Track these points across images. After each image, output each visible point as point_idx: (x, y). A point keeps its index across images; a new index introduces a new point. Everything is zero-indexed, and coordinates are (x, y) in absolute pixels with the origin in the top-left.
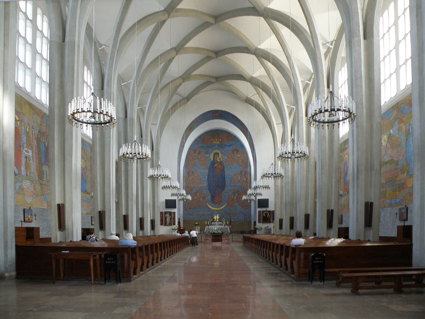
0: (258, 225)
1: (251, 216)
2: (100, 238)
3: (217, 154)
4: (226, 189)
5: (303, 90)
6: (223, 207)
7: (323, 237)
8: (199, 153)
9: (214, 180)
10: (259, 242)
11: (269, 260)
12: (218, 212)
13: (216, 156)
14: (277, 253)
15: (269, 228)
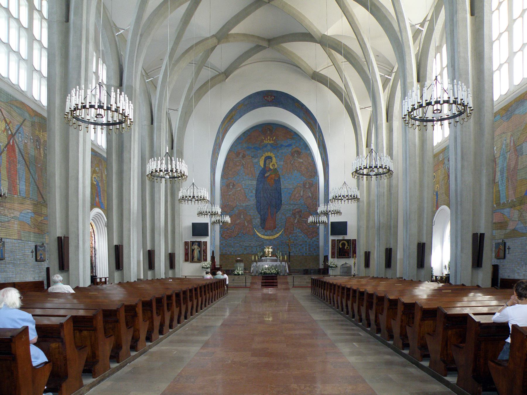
0: (331, 261)
1: (318, 247)
2: (116, 282)
3: (270, 158)
4: (282, 208)
5: (413, 37)
6: (278, 235)
7: (412, 280)
8: (244, 157)
9: (265, 195)
10: (333, 287)
11: (342, 311)
12: (270, 243)
13: (267, 162)
14: (327, 291)
15: (348, 265)
